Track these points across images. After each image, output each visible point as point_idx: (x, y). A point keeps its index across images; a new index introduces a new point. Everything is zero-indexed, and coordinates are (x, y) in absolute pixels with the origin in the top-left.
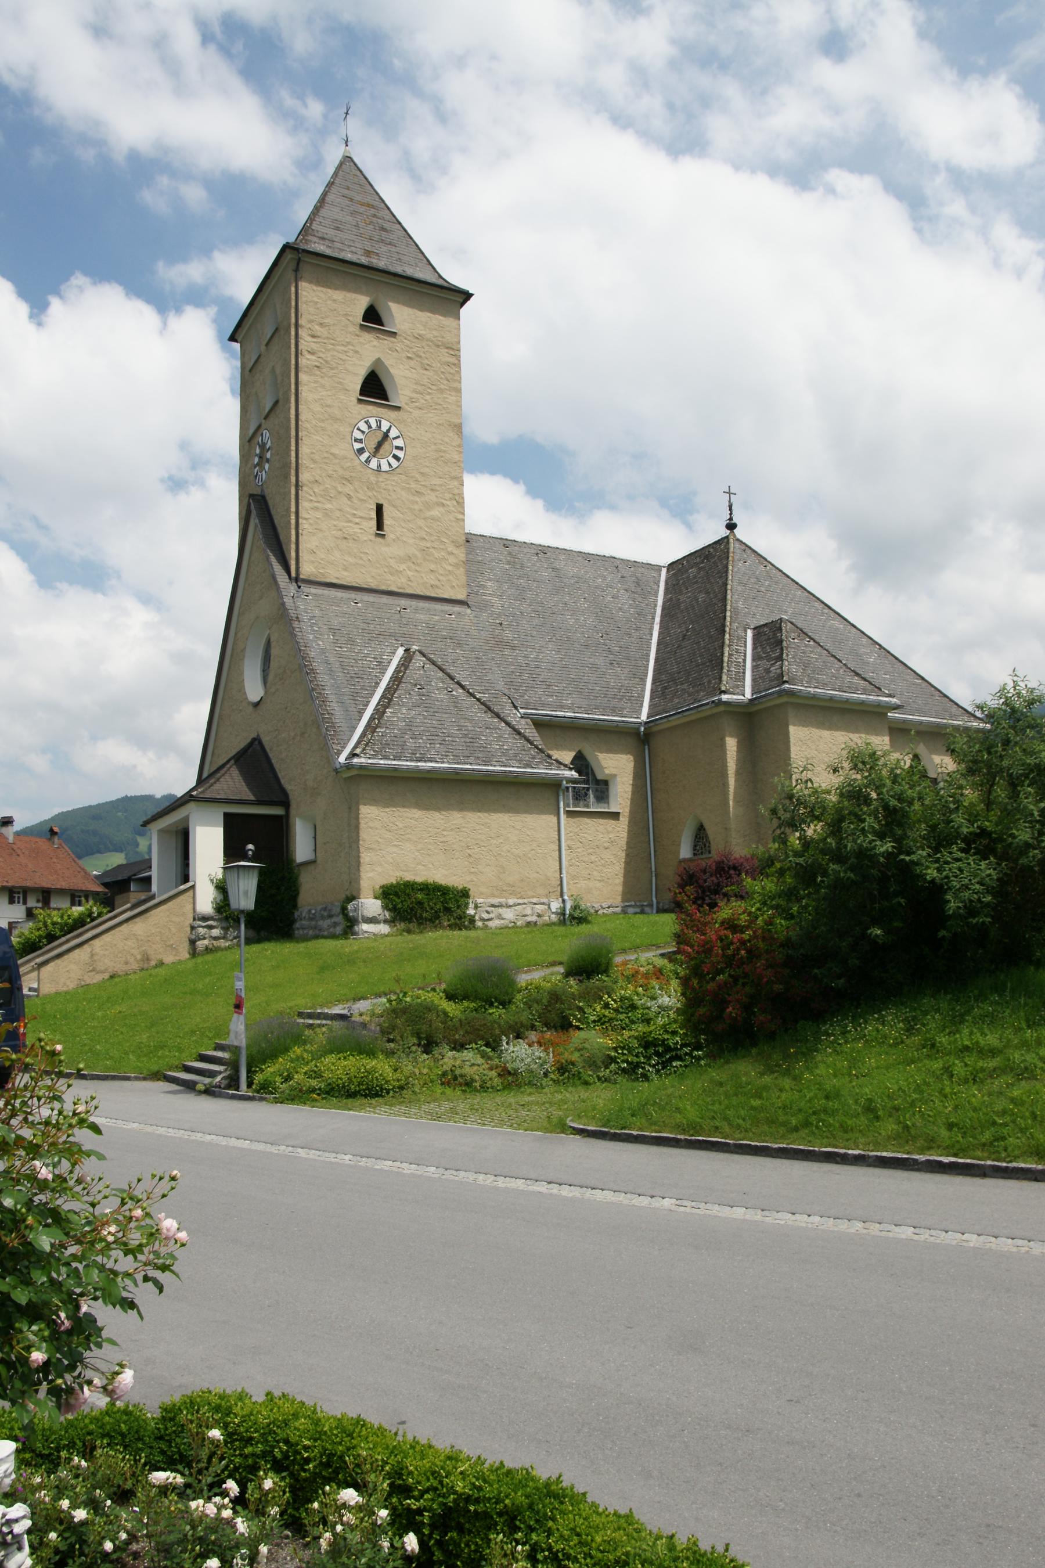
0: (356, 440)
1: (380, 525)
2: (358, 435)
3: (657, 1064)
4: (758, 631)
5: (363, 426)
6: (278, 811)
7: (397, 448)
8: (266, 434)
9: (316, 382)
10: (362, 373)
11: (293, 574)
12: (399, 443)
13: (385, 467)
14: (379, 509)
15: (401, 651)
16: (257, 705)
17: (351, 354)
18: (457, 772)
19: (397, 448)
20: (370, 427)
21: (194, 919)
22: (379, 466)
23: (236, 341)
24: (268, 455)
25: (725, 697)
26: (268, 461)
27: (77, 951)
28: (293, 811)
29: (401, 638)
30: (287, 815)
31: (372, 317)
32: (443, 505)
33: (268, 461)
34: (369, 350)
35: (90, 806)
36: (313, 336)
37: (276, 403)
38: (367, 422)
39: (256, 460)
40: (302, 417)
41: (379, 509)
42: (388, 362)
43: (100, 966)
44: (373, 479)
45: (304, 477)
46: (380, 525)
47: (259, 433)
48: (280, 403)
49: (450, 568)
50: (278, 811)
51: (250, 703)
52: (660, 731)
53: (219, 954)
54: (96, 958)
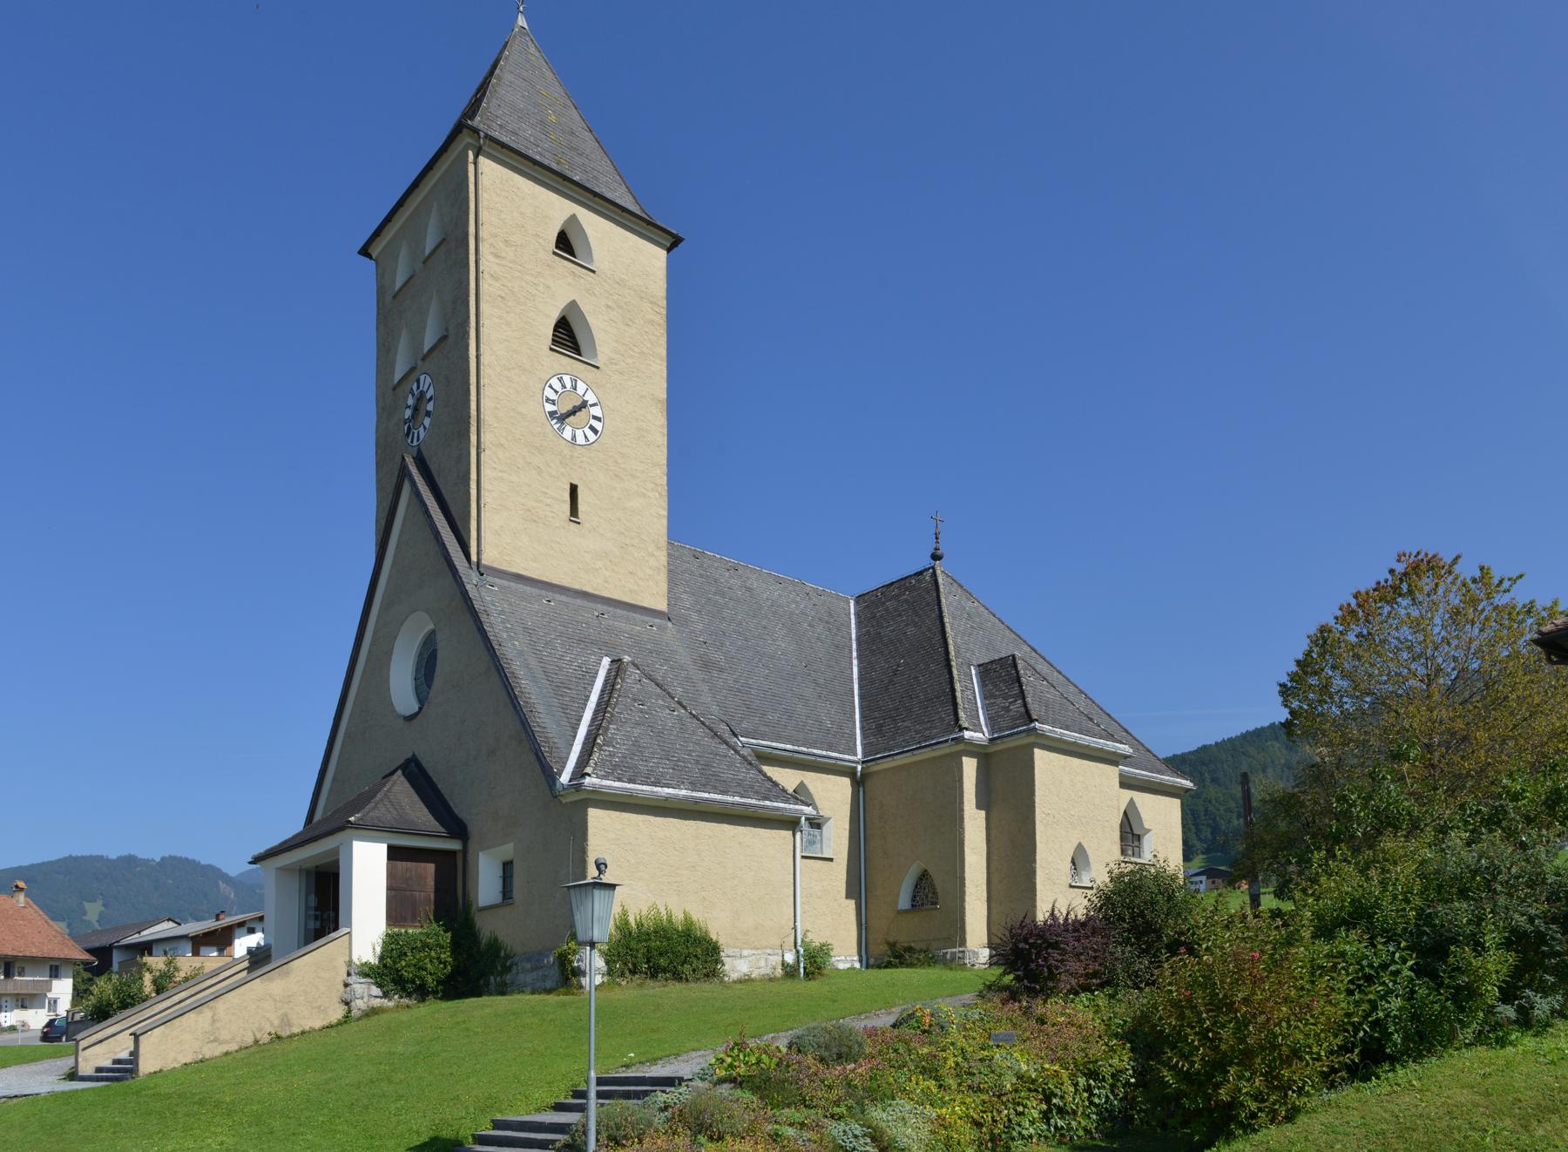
0: (548, 400)
1: (574, 510)
2: (549, 393)
3: (1096, 1106)
4: (985, 671)
5: (557, 386)
6: (454, 845)
7: (595, 418)
8: (426, 381)
9: (500, 317)
10: (554, 317)
11: (474, 558)
12: (596, 411)
13: (580, 440)
14: (574, 490)
15: (606, 661)
16: (410, 718)
17: (541, 288)
18: (696, 801)
19: (595, 418)
20: (564, 386)
21: (349, 974)
22: (574, 437)
23: (370, 256)
24: (430, 407)
25: (967, 734)
26: (428, 414)
27: (191, 1015)
28: (472, 845)
29: (605, 647)
30: (465, 851)
31: (565, 243)
32: (644, 495)
33: (428, 414)
34: (560, 287)
35: (20, 867)
36: (497, 256)
37: (444, 338)
38: (560, 380)
39: (408, 413)
40: (484, 360)
41: (574, 490)
42: (585, 308)
43: (225, 1035)
44: (566, 452)
45: (487, 438)
46: (574, 510)
47: (414, 376)
48: (451, 340)
49: (649, 572)
50: (454, 845)
51: (399, 716)
52: (878, 772)
53: (385, 1016)
54: (218, 1025)
